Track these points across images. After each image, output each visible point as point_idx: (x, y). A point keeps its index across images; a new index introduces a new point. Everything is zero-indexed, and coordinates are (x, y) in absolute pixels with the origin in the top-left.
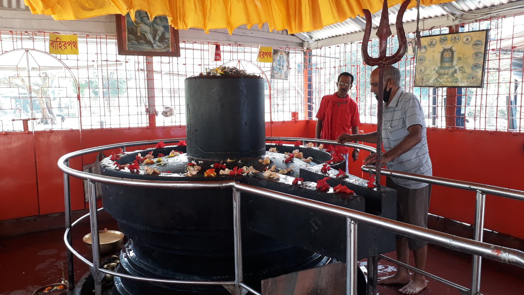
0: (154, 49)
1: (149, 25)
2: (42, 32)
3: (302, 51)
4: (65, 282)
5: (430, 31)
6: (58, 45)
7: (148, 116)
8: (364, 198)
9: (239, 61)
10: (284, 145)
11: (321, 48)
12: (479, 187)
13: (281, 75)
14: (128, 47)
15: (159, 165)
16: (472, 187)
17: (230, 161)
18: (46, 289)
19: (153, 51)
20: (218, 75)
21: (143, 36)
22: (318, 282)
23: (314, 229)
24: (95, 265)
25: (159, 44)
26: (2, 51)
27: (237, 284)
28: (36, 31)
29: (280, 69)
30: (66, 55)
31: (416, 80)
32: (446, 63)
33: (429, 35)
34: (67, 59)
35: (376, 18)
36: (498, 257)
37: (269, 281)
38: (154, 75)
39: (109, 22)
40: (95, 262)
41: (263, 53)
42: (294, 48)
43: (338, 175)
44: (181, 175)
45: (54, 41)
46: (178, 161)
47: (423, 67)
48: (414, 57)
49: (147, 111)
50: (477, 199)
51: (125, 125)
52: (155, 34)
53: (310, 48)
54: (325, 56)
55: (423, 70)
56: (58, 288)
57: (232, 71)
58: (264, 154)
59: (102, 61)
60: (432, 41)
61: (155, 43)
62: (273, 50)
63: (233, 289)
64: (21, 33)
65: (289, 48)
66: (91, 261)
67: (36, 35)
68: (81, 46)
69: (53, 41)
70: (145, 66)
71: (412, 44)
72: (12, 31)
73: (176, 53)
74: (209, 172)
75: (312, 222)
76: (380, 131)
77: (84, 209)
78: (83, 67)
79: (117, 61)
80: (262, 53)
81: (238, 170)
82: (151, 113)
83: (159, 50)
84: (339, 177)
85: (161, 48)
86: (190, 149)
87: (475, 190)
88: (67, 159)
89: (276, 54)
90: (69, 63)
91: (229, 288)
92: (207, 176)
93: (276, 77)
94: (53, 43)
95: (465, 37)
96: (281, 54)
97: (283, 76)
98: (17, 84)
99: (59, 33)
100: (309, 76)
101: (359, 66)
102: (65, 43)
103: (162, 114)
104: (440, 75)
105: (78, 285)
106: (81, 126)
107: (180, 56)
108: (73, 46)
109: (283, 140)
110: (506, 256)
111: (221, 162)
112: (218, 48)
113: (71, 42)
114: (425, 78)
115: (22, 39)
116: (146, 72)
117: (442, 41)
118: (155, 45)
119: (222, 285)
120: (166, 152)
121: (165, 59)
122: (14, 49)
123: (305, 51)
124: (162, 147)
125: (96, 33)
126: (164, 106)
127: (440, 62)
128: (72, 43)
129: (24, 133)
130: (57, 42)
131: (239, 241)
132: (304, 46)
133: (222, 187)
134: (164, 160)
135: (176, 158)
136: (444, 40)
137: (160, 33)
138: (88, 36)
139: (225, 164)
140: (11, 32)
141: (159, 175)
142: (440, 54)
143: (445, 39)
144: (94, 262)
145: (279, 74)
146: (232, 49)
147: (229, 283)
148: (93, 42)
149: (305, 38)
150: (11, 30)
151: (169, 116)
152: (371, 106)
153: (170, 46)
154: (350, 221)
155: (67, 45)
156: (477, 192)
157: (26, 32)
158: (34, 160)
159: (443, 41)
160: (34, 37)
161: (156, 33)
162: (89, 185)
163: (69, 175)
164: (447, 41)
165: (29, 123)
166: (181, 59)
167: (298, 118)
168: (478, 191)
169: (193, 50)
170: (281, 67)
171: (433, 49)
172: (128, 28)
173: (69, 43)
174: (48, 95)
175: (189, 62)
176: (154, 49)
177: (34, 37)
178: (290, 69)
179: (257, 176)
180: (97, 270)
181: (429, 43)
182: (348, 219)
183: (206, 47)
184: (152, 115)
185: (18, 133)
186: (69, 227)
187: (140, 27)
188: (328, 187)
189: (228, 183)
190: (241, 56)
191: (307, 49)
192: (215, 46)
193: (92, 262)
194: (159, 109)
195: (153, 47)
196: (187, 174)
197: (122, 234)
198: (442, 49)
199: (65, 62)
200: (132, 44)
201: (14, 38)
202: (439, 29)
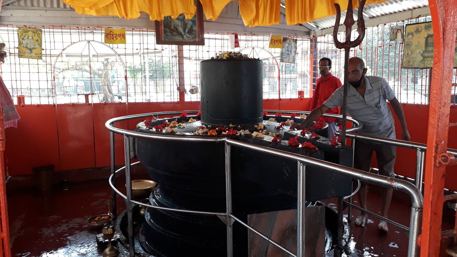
0: (184, 39)
2: (99, 27)
3: (308, 38)
4: (110, 214)
5: (417, 19)
6: (111, 37)
7: (179, 93)
8: (324, 152)
9: (253, 48)
10: (283, 116)
11: (324, 36)
12: (418, 146)
13: (289, 59)
15: (179, 128)
16: (414, 146)
17: (232, 126)
18: (97, 218)
19: (184, 41)
20: (224, 58)
21: (176, 29)
22: (294, 221)
23: (286, 175)
24: (128, 198)
25: (188, 35)
26: (71, 42)
27: (228, 215)
28: (95, 26)
29: (288, 54)
30: (117, 44)
31: (403, 62)
32: (430, 47)
33: (416, 23)
34: (118, 48)
35: (371, 9)
36: (391, 185)
37: (254, 216)
38: (184, 60)
40: (128, 195)
41: (274, 41)
42: (302, 36)
43: (311, 136)
44: (191, 134)
45: (108, 33)
47: (410, 51)
48: (402, 42)
49: (178, 89)
50: (417, 156)
51: (161, 100)
52: (185, 27)
53: (316, 36)
54: (328, 42)
55: (410, 54)
56: (105, 217)
57: (236, 55)
59: (143, 49)
60: (418, 28)
61: (185, 34)
62: (283, 38)
63: (225, 218)
64: (147, 30)
65: (297, 36)
66: (126, 195)
67: (95, 29)
68: (128, 38)
69: (107, 34)
70: (177, 53)
71: (401, 32)
72: (78, 27)
73: (202, 43)
74: (212, 131)
75: (284, 170)
76: (345, 102)
78: (129, 55)
79: (155, 49)
80: (273, 41)
81: (233, 131)
82: (181, 91)
83: (188, 40)
84: (312, 138)
85: (190, 39)
86: (203, 117)
87: (416, 148)
88: (113, 122)
89: (285, 42)
90: (119, 51)
91: (221, 218)
92: (210, 135)
93: (285, 61)
94: (107, 35)
96: (290, 41)
98: (85, 70)
99: (112, 28)
100: (314, 59)
101: (356, 51)
102: (116, 35)
103: (189, 91)
104: (424, 57)
105: (120, 217)
106: (128, 100)
107: (204, 45)
109: (282, 113)
110: (396, 185)
111: (225, 126)
112: (236, 37)
113: (121, 34)
114: (411, 60)
115: (85, 33)
116: (177, 58)
117: (427, 28)
118: (185, 36)
119: (216, 215)
120: (186, 120)
121: (193, 47)
122: (80, 41)
123: (311, 38)
124: (185, 116)
125: (140, 27)
126: (191, 85)
127: (425, 46)
128: (121, 35)
129: (85, 104)
130: (110, 34)
131: (229, 182)
132: (310, 34)
133: (217, 141)
134: (184, 125)
136: (429, 27)
137: (189, 26)
138: (133, 29)
139: (228, 128)
140: (78, 27)
141: (176, 134)
142: (425, 39)
143: (429, 26)
144: (127, 195)
145: (288, 58)
146: (247, 38)
148: (137, 34)
149: (312, 27)
150: (78, 26)
151: (195, 93)
153: (197, 37)
154: (299, 163)
156: (418, 149)
157: (88, 27)
158: (93, 126)
159: (427, 28)
160: (94, 31)
161: (186, 27)
162: (124, 138)
163: (114, 132)
164: (431, 28)
165: (90, 96)
166: (205, 48)
167: (304, 96)
168: (418, 149)
169: (258, 41)
170: (289, 52)
171: (419, 35)
172: (164, 23)
173: (119, 35)
174: (108, 79)
176: (184, 39)
177: (94, 31)
178: (298, 54)
179: (247, 136)
180: (129, 201)
181: (416, 29)
182: (298, 162)
183: (226, 37)
184: (182, 93)
185: (81, 105)
186: (113, 173)
188: (298, 144)
189: (221, 139)
190: (255, 44)
191: (313, 36)
192: (234, 35)
194: (188, 88)
195: (183, 37)
196: (195, 133)
197: (154, 183)
198: (427, 35)
199: (116, 50)
200: (167, 35)
201: (80, 32)
202: (425, 17)
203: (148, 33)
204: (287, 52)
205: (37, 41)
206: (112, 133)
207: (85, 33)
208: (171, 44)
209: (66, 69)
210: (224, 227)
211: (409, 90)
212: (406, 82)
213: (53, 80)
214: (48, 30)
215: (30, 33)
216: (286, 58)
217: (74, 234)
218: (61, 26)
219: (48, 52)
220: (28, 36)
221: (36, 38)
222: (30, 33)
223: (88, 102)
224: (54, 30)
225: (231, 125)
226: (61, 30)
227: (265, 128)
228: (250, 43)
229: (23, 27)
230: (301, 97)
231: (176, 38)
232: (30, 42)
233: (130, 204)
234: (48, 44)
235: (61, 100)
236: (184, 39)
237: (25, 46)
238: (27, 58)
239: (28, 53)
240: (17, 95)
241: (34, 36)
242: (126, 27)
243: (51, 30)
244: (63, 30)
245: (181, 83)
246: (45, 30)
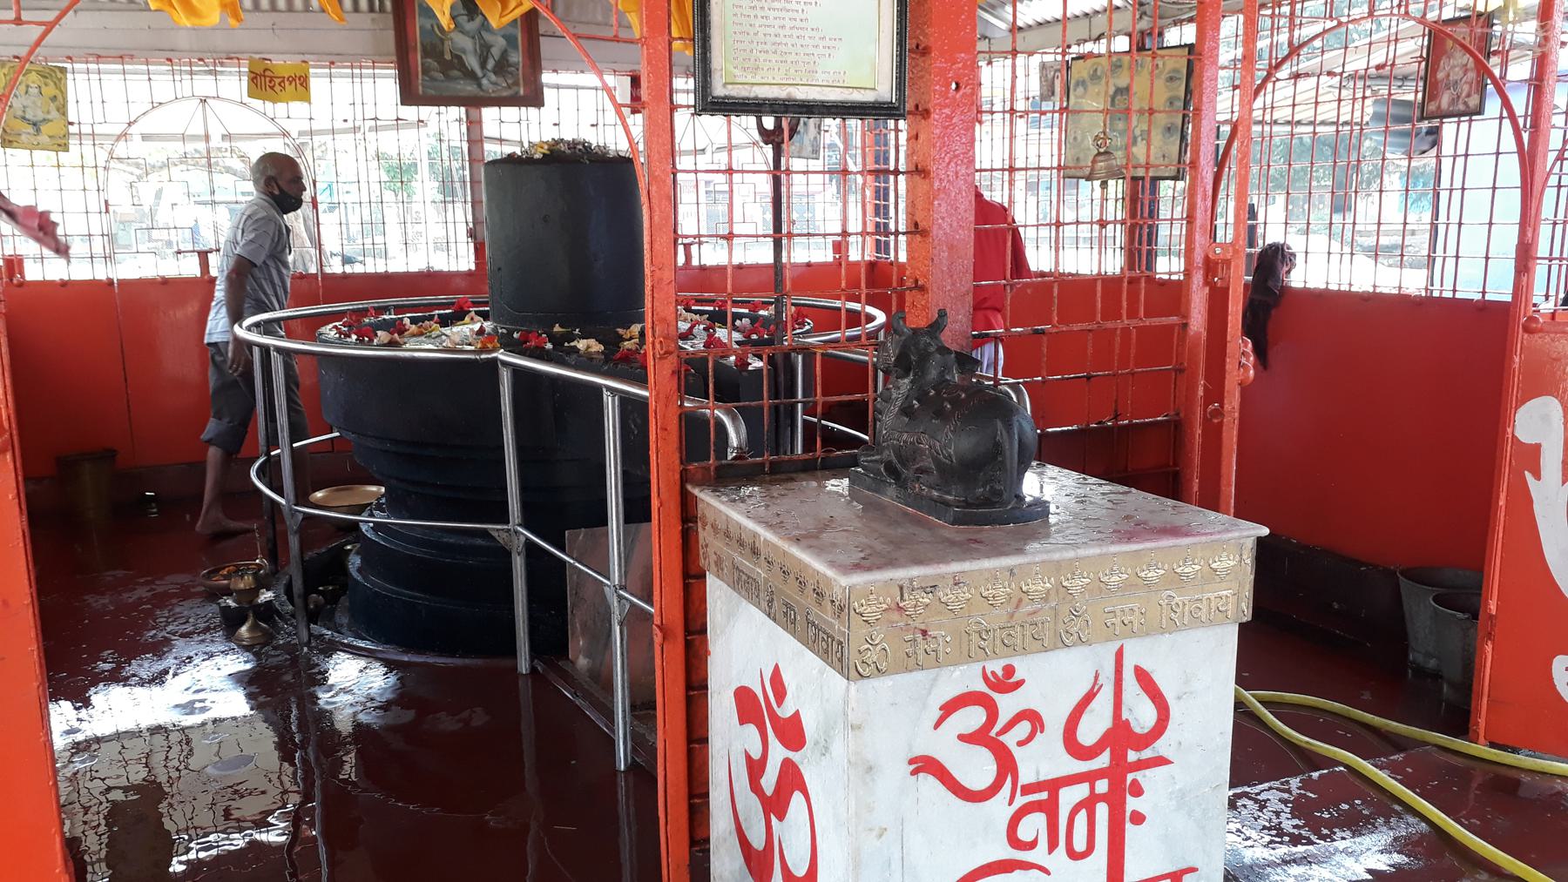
0: (482, 90)
1: (471, 34)
2: (231, 57)
7: (472, 246)
13: (801, 149)
14: (423, 87)
17: (561, 330)
19: (482, 93)
20: (537, 156)
21: (458, 62)
24: (288, 501)
25: (493, 78)
28: (219, 55)
39: (380, 29)
61: (484, 76)
66: (281, 494)
67: (222, 64)
68: (318, 84)
77: (330, 449)
79: (398, 119)
82: (479, 240)
108: (298, 85)
115: (191, 73)
118: (484, 81)
121: (510, 112)
130: (265, 76)
137: (496, 52)
138: (333, 63)
140: (170, 60)
150: (169, 55)
152: (1405, 224)
153: (521, 82)
155: (287, 83)
157: (200, 60)
165: (694, 249)
172: (422, 44)
176: (482, 90)
180: (291, 509)
187: (451, 39)
192: (629, 78)
193: (283, 497)
195: (480, 85)
200: (433, 79)
203: (377, 71)
205: (54, 98)
206: (256, 350)
207: (191, 73)
208: (446, 105)
209: (160, 164)
210: (507, 555)
211: (1315, 232)
212: (1306, 206)
213: (104, 210)
214: (84, 66)
215: (33, 76)
217: (167, 606)
218: (121, 57)
219: (86, 129)
220: (28, 86)
221: (50, 90)
222: (33, 76)
223: (209, 272)
224: (101, 66)
225: (557, 328)
226: (120, 67)
229: (12, 59)
231: (459, 87)
232: (34, 103)
233: (293, 515)
234: (85, 106)
235: (130, 268)
236: (484, 88)
237: (20, 113)
238: (26, 148)
239: (29, 133)
240: (3, 255)
241: (43, 86)
242: (312, 57)
243: (93, 66)
244: (127, 67)
245: (477, 215)
246: (77, 66)
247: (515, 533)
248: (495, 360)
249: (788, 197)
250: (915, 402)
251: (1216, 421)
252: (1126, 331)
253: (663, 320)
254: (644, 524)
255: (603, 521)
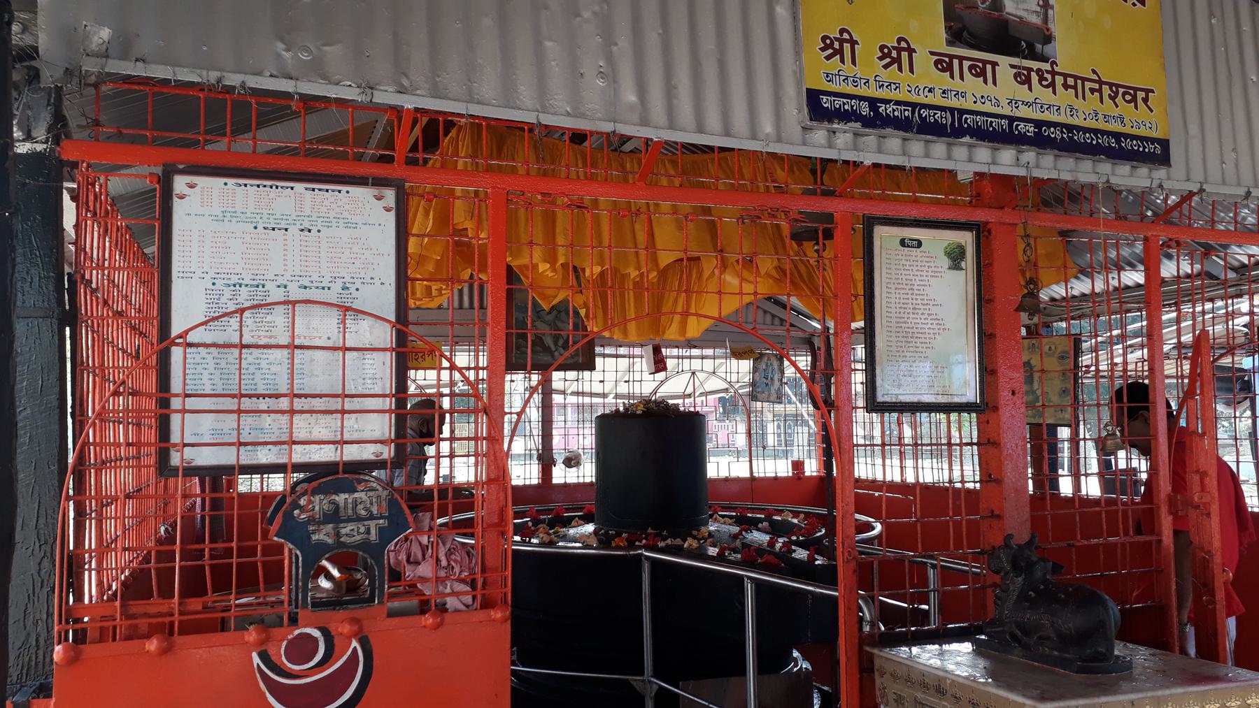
9: (693, 373)
17: (652, 531)
20: (638, 412)
29: (767, 385)
46: (583, 531)
58: (706, 524)
87: (926, 563)
95: (1047, 344)
96: (769, 359)
97: (773, 397)
109: (749, 508)
118: (556, 354)
120: (567, 523)
121: (571, 375)
135: (579, 528)
147: (638, 678)
166: (597, 375)
175: (610, 377)
195: (553, 356)
204: (765, 380)
216: (763, 392)
225: (650, 531)
227: (710, 535)
228: (686, 361)
230: (797, 473)
247: (649, 682)
248: (641, 555)
249: (839, 443)
250: (1030, 593)
251: (1210, 607)
252: (1123, 545)
253: (848, 537)
254: (733, 680)
255: (743, 672)
